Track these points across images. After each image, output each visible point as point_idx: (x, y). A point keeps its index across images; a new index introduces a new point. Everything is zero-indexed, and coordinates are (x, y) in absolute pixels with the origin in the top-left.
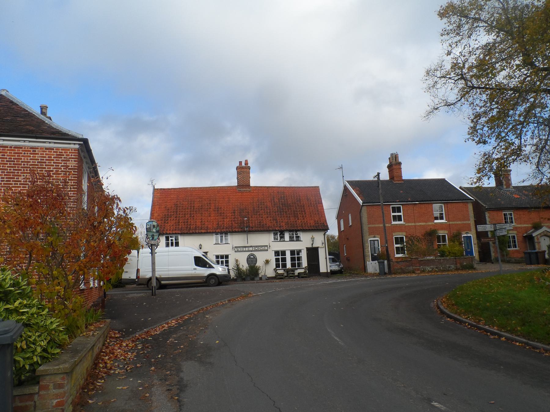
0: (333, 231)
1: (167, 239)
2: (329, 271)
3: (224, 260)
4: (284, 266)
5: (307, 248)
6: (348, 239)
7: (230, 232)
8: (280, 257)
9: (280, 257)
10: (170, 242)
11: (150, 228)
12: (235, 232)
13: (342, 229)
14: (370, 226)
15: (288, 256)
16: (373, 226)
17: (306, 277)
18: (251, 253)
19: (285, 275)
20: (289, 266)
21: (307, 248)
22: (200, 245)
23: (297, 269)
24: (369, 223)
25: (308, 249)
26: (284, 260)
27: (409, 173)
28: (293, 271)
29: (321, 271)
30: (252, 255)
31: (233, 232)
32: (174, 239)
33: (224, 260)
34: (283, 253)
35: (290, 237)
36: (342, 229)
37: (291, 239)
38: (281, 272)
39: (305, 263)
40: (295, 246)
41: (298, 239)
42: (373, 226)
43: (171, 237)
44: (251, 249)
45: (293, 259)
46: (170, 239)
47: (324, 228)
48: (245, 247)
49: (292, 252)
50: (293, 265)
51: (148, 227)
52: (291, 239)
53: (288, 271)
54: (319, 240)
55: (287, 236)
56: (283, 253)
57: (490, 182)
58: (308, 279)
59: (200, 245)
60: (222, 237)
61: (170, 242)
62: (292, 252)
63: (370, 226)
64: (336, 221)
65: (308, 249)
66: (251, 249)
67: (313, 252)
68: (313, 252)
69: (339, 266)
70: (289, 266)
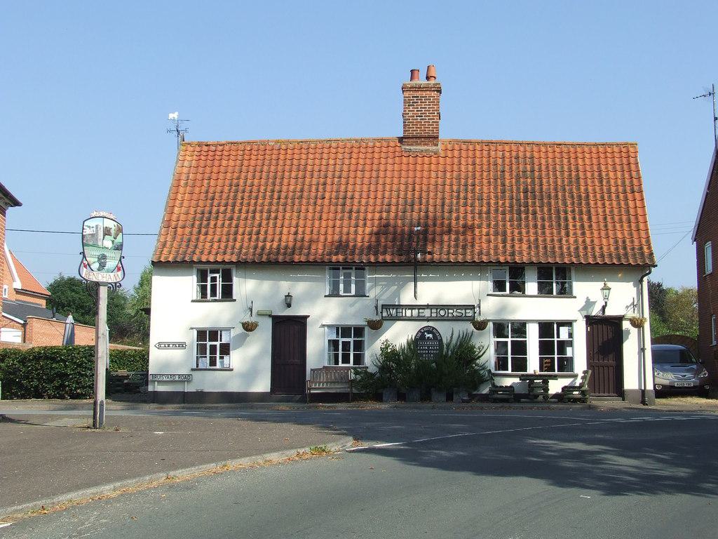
0: (678, 269)
2: (650, 386)
3: (351, 340)
4: (520, 365)
8: (509, 340)
10: (209, 284)
13: (709, 268)
14: (513, 339)
18: (425, 324)
20: (533, 365)
22: (289, 296)
23: (555, 377)
26: (520, 348)
27: (459, 122)
28: (545, 380)
30: (431, 330)
33: (351, 340)
34: (520, 328)
36: (709, 268)
37: (545, 290)
39: (579, 355)
40: (553, 308)
41: (565, 292)
43: (212, 272)
44: (427, 313)
45: (545, 348)
47: (635, 265)
49: (546, 328)
50: (546, 365)
54: (621, 298)
55: (532, 287)
56: (520, 328)
59: (289, 296)
60: (348, 276)
62: (546, 328)
63: (513, 339)
64: (693, 248)
66: (427, 313)
67: (606, 334)
68: (606, 334)
69: (697, 373)
70: (533, 365)
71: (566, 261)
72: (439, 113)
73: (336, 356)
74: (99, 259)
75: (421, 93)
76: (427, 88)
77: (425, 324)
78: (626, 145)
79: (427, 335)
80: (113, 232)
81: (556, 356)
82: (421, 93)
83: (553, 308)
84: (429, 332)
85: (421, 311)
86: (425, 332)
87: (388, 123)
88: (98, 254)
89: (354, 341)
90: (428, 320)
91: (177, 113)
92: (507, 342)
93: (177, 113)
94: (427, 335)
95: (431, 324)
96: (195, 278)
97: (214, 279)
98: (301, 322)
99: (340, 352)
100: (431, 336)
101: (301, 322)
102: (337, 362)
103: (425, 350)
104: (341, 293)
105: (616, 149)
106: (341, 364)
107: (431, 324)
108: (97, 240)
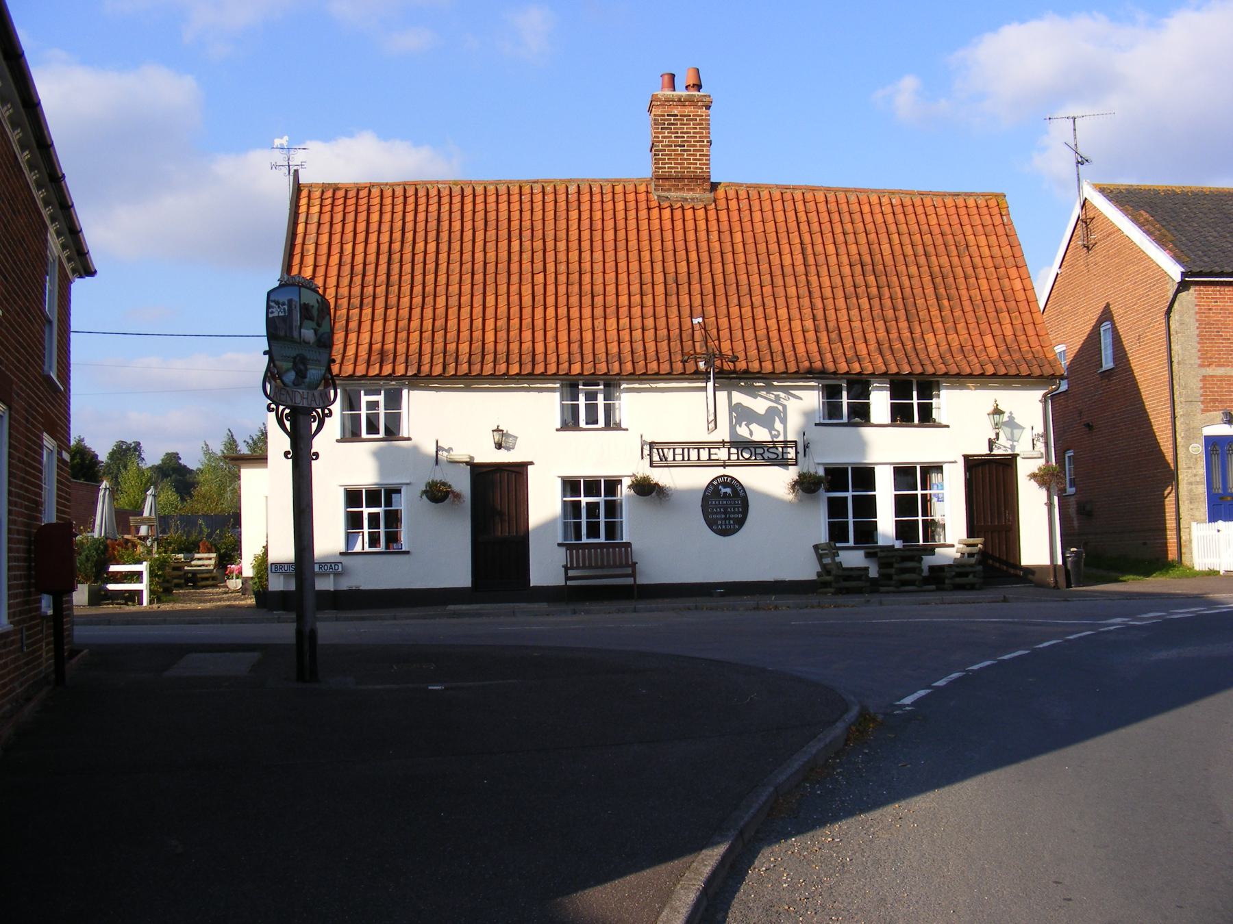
1: (351, 403)
3: (601, 500)
4: (867, 532)
5: (966, 457)
6: (1088, 425)
7: (633, 377)
8: (849, 495)
9: (849, 495)
10: (364, 412)
11: (287, 319)
12: (657, 376)
13: (934, 587)
14: (1209, 371)
15: (885, 493)
16: (1220, 371)
17: (972, 587)
18: (720, 471)
19: (873, 573)
21: (966, 457)
24: (1206, 359)
25: (973, 465)
26: (867, 507)
29: (534, 582)
31: (645, 376)
32: (381, 398)
33: (601, 500)
34: (865, 476)
35: (894, 408)
37: (901, 415)
38: (853, 558)
40: (912, 445)
42: (1220, 371)
45: (904, 505)
46: (365, 399)
48: (699, 446)
49: (904, 474)
50: (905, 530)
51: (276, 312)
52: (901, 415)
53: (883, 556)
57: (317, 569)
58: (875, 598)
61: (364, 412)
62: (904, 474)
63: (1209, 371)
65: (973, 465)
67: (990, 479)
71: (930, 370)
72: (710, 142)
73: (578, 527)
74: (295, 364)
75: (681, 113)
76: (690, 101)
77: (720, 471)
78: (996, 196)
79: (723, 490)
80: (315, 313)
81: (920, 518)
82: (681, 113)
83: (912, 445)
84: (725, 485)
85: (713, 451)
86: (719, 484)
87: (627, 158)
88: (293, 353)
89: (606, 502)
90: (724, 466)
91: (286, 138)
92: (846, 498)
93: (286, 138)
94: (723, 490)
95: (730, 471)
96: (557, 396)
97: (373, 405)
98: (518, 472)
99: (602, 520)
100: (728, 490)
101: (518, 472)
102: (579, 537)
103: (720, 513)
104: (582, 424)
105: (981, 202)
106: (584, 540)
107: (730, 471)
108: (291, 328)
